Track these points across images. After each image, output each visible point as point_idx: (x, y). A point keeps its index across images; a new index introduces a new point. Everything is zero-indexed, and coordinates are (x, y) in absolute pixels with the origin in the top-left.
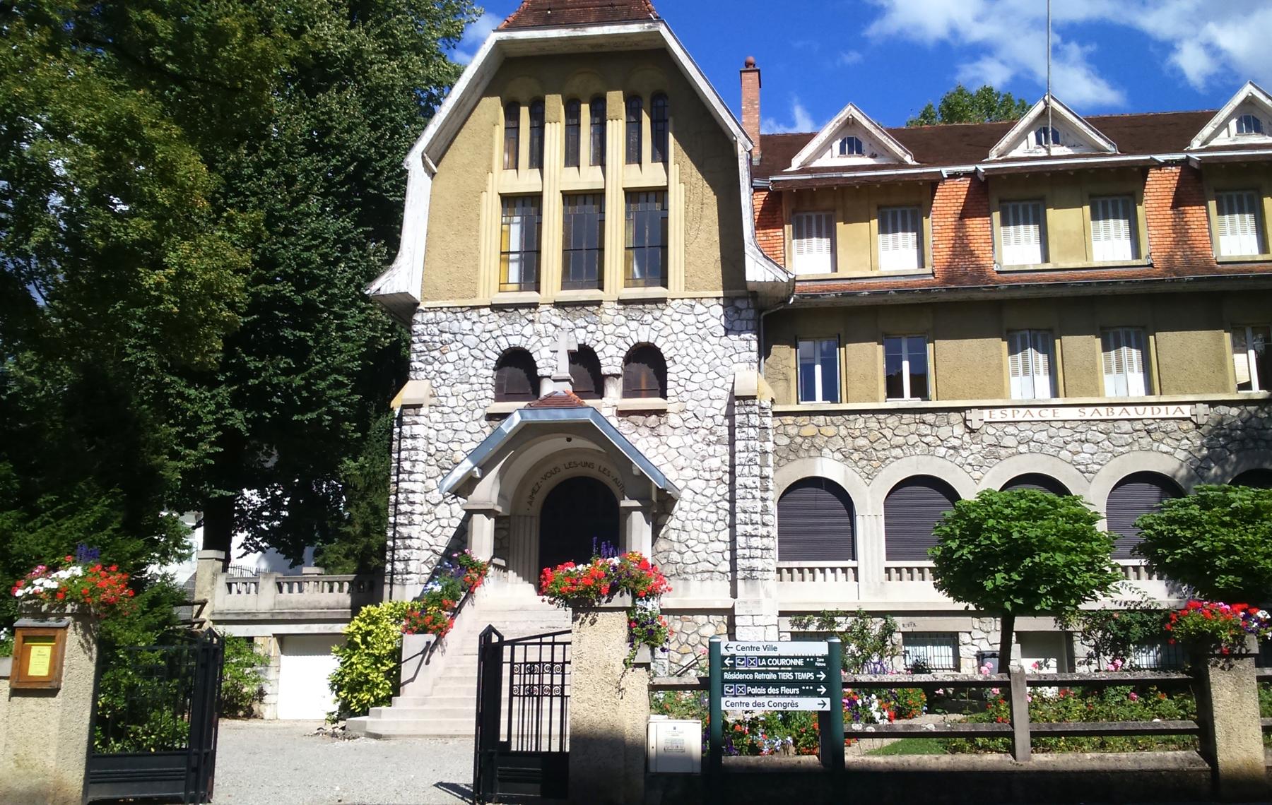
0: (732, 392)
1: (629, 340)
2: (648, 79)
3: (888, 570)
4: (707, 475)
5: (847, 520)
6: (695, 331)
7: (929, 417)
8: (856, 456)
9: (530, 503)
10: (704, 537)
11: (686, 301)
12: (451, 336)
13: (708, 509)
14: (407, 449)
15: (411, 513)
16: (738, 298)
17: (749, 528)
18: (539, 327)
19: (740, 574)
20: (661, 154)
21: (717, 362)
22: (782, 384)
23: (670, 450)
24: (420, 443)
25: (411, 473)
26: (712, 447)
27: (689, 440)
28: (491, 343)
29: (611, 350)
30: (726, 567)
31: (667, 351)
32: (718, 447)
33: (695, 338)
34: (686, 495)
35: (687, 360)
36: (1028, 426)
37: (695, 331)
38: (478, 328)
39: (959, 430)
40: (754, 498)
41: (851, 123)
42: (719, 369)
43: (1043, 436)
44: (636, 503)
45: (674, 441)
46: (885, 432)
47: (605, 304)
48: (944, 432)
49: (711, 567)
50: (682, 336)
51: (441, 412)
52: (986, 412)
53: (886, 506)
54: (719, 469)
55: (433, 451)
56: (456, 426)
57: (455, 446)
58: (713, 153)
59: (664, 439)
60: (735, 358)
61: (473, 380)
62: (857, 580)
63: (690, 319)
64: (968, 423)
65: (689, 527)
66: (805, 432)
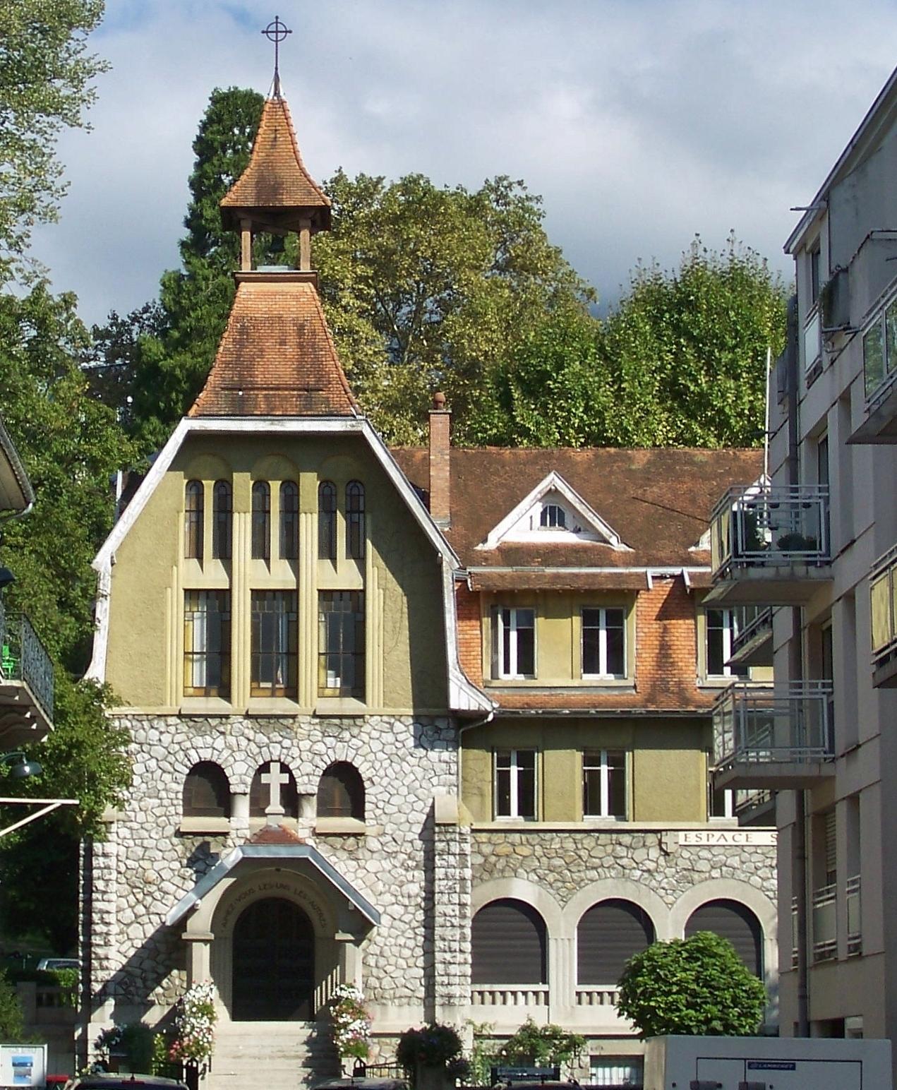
0: (431, 815)
1: (325, 758)
2: (344, 467)
3: (579, 994)
4: (406, 901)
5: (538, 942)
6: (394, 751)
7: (626, 839)
8: (551, 878)
9: (224, 925)
10: (402, 962)
11: (385, 719)
12: (137, 747)
13: (407, 935)
14: (99, 868)
15: (107, 934)
16: (438, 717)
17: (448, 956)
18: (232, 740)
19: (438, 1001)
20: (357, 554)
21: (417, 784)
22: (476, 801)
23: (372, 872)
24: (112, 862)
25: (104, 892)
26: (411, 873)
27: (387, 865)
28: (181, 755)
29: (308, 768)
30: (421, 992)
31: (365, 770)
32: (416, 873)
33: (395, 758)
34: (385, 920)
35: (385, 781)
36: (722, 850)
37: (394, 751)
38: (166, 739)
39: (655, 853)
40: (453, 926)
41: (553, 493)
42: (419, 792)
43: (735, 861)
44: (350, 937)
45: (372, 865)
46: (582, 853)
47: (300, 719)
48: (640, 854)
49: (409, 993)
50: (381, 756)
51: (131, 829)
52: (682, 834)
53: (579, 928)
54: (417, 895)
55: (123, 869)
56: (146, 843)
57: (146, 864)
58: (415, 562)
59: (362, 863)
60: (435, 780)
61: (163, 794)
62: (547, 1003)
63: (389, 738)
64: (664, 846)
65: (387, 952)
66: (500, 850)
